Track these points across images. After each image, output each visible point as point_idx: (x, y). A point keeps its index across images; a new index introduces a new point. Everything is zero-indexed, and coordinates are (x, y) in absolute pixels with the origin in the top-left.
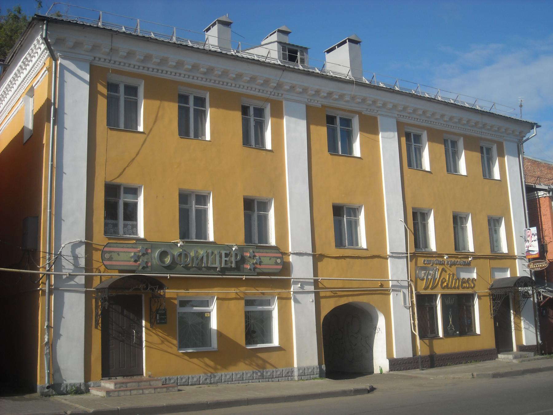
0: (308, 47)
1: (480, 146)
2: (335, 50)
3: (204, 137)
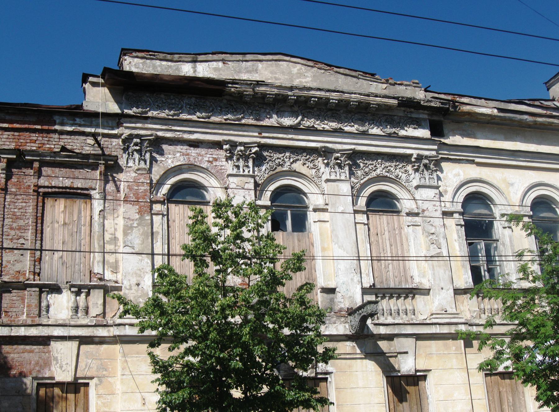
2: (106, 67)
3: (115, 124)
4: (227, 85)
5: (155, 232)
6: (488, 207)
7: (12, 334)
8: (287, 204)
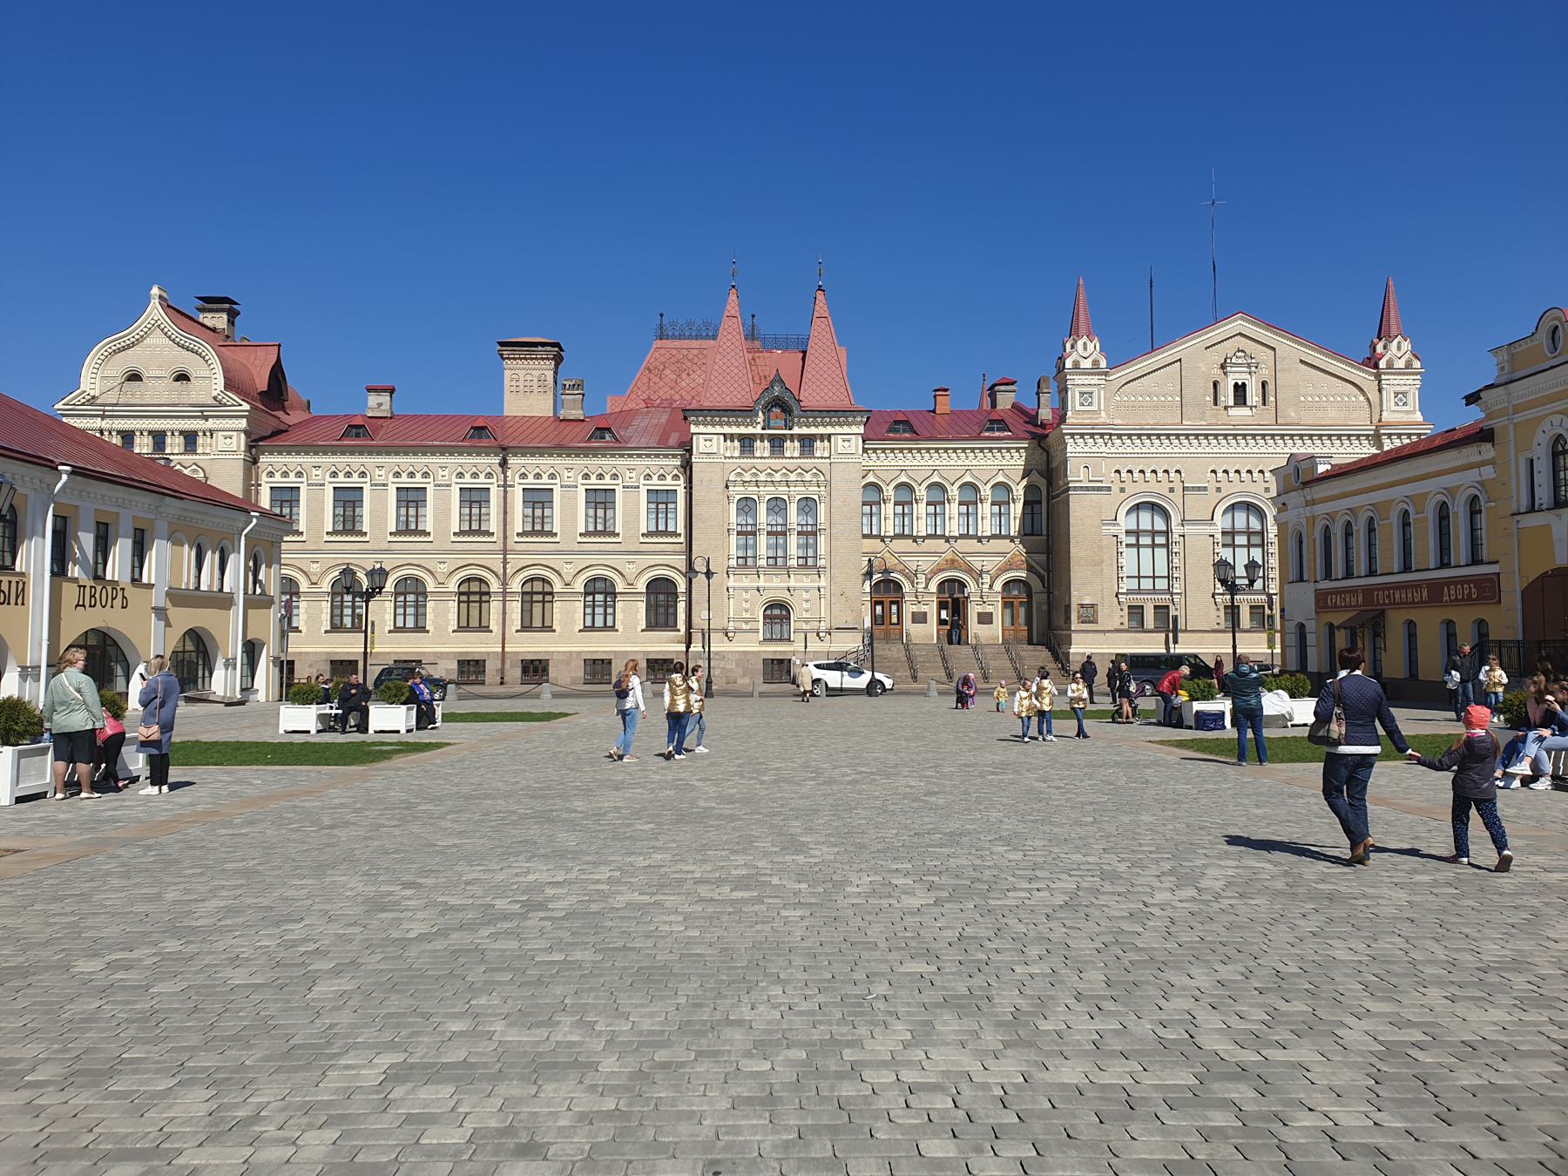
3: (1030, 499)
5: (953, 694)
6: (548, 675)
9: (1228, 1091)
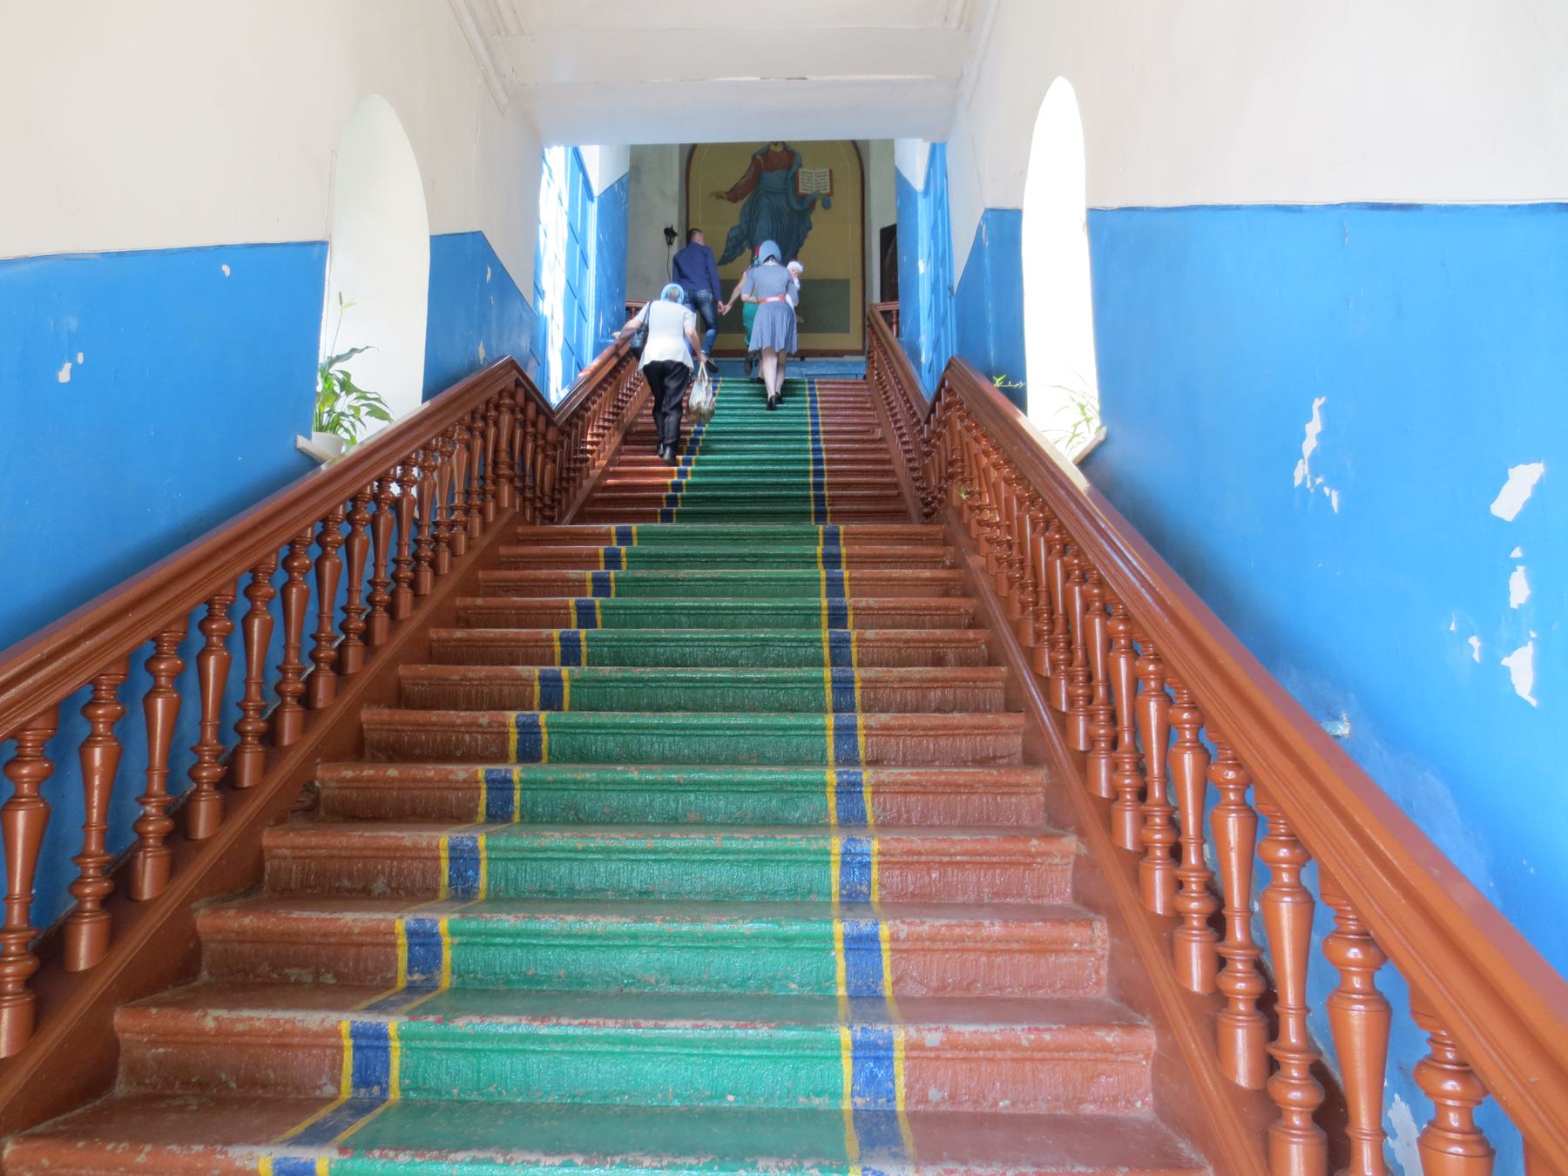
0: (1082, 216)
1: (323, 245)
3: (455, 359)
4: (966, 521)
7: (1045, 434)
8: (23, 685)
9: (676, 672)
